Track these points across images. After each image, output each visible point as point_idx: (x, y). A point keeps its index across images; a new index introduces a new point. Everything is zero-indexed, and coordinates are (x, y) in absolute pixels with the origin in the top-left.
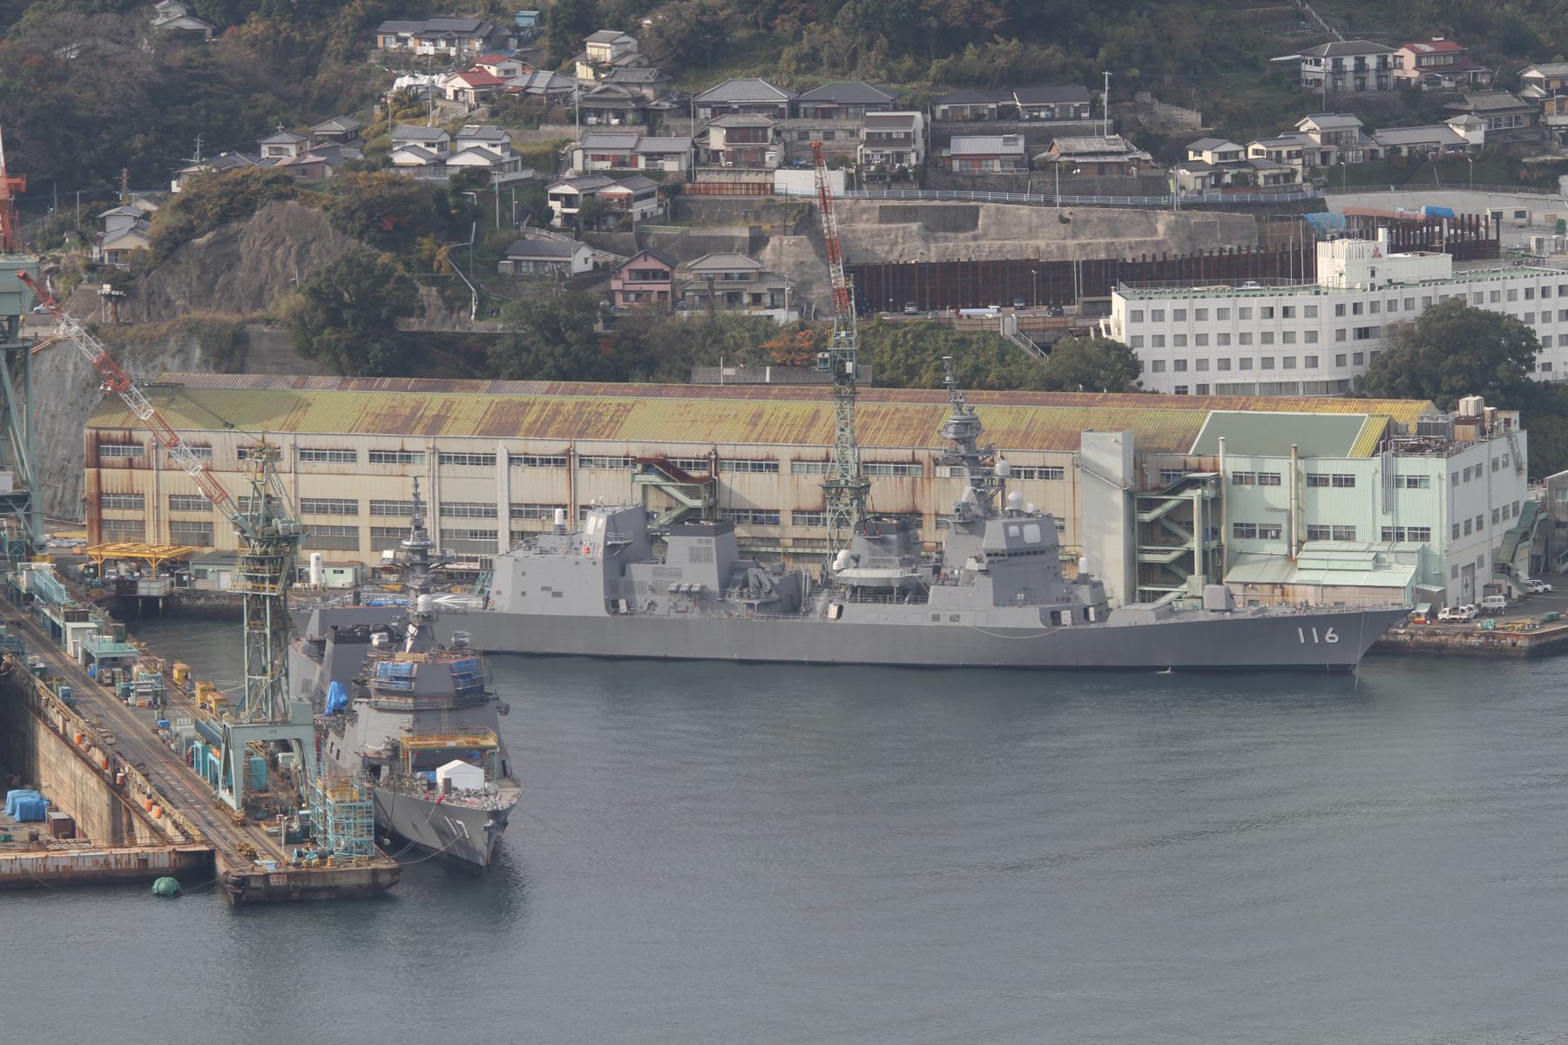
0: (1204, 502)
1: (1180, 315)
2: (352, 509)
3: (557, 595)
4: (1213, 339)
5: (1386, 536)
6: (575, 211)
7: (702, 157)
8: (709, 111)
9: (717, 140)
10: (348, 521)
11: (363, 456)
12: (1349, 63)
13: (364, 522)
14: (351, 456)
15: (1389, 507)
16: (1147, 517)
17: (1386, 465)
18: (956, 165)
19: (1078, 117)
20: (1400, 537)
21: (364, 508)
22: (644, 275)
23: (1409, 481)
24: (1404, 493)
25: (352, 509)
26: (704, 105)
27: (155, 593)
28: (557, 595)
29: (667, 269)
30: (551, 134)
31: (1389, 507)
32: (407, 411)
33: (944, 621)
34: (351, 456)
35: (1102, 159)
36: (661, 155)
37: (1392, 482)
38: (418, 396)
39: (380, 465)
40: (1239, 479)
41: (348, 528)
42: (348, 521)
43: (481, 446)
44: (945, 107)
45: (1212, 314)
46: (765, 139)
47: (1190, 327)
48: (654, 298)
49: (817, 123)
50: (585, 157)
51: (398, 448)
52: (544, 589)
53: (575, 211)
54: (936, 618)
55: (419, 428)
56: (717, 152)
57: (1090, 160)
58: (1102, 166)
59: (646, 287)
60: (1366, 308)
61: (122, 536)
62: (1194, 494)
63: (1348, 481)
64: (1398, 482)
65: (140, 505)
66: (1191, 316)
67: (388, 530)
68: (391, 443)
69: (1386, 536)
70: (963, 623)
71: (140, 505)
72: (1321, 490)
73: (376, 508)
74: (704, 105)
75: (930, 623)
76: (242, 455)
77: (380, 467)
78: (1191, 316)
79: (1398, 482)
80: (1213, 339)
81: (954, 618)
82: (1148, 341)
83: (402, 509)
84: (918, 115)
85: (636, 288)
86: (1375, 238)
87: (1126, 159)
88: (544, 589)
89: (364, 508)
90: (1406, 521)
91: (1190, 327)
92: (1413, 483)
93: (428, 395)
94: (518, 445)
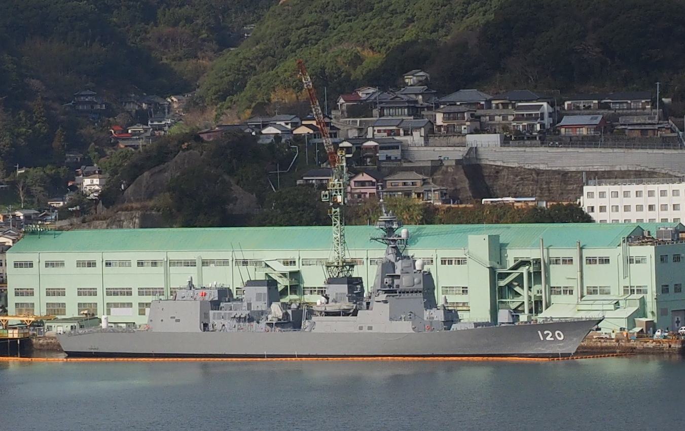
0: (529, 274)
1: (616, 195)
3: (178, 321)
4: (633, 208)
5: (626, 291)
6: (350, 156)
13: (135, 299)
16: (502, 283)
17: (625, 251)
18: (563, 130)
20: (632, 291)
21: (135, 292)
22: (363, 184)
27: (16, 336)
28: (178, 321)
29: (374, 180)
33: (365, 330)
35: (643, 127)
44: (569, 102)
45: (633, 194)
46: (464, 118)
47: (621, 201)
48: (367, 196)
50: (374, 131)
52: (171, 318)
54: (361, 328)
57: (637, 127)
59: (363, 191)
61: (24, 312)
63: (607, 261)
64: (631, 261)
65: (32, 294)
66: (621, 195)
69: (62, 264)
70: (374, 330)
71: (32, 294)
75: (357, 331)
79: (631, 261)
80: (633, 208)
81: (370, 328)
82: (597, 209)
83: (153, 292)
85: (358, 191)
87: (656, 127)
88: (171, 318)
89: (135, 292)
90: (635, 283)
91: (621, 201)
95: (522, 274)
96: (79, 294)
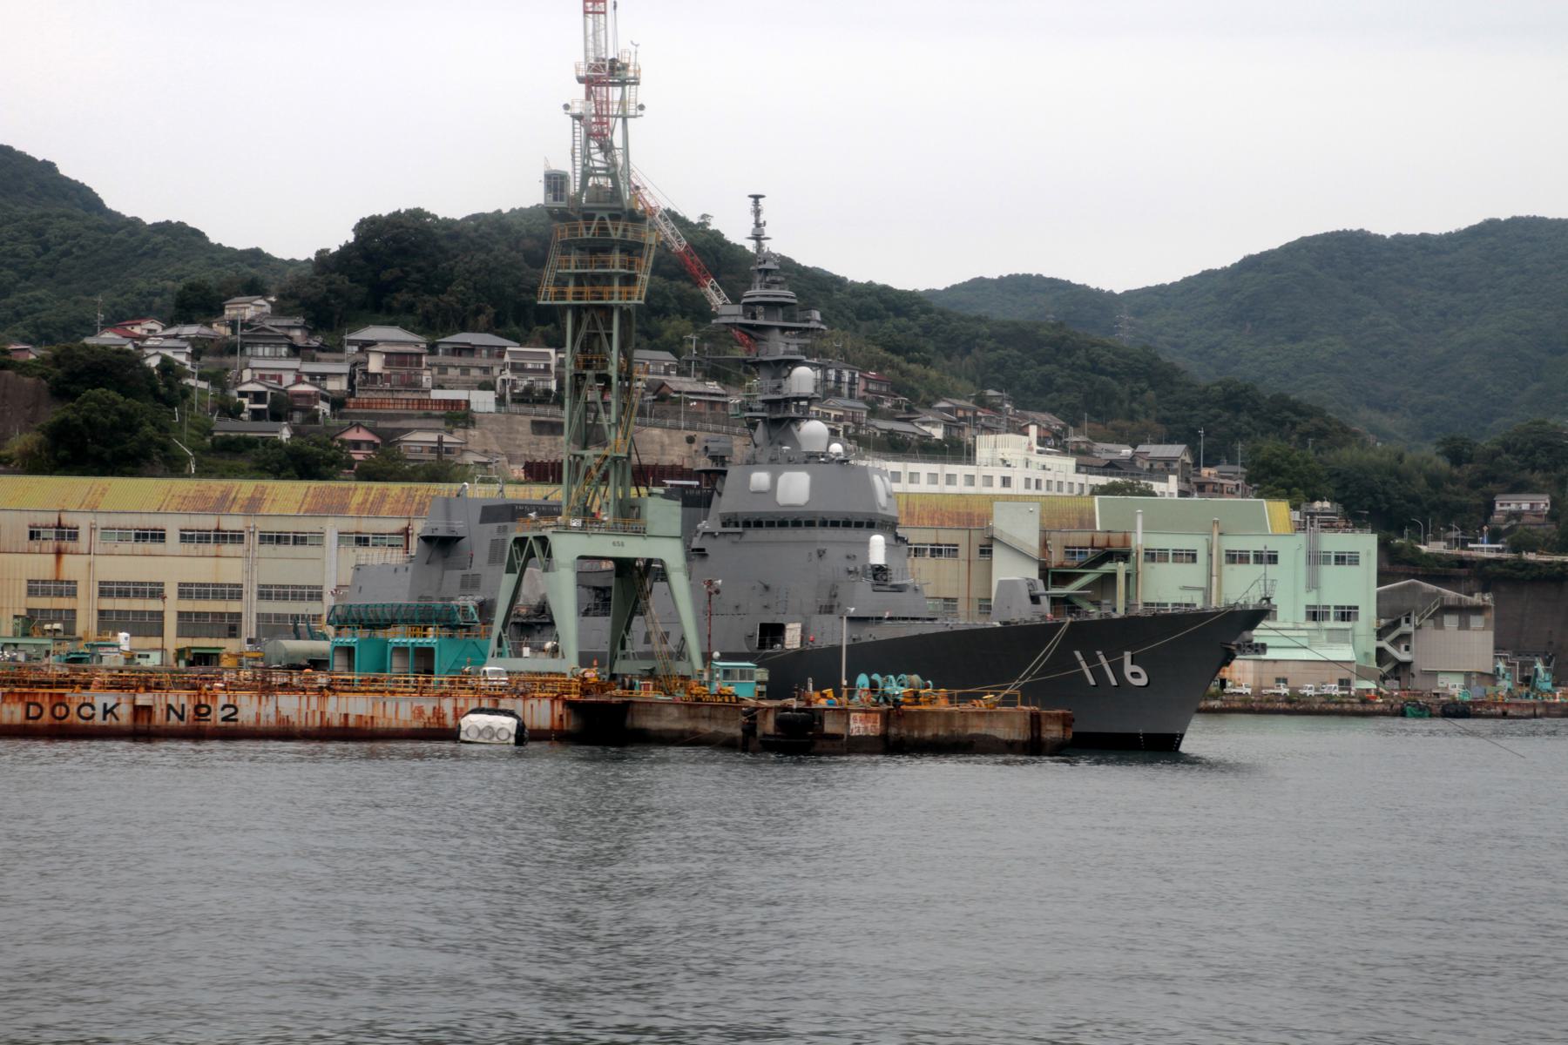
2: (157, 592)
7: (359, 378)
8: (356, 348)
9: (375, 364)
10: (153, 605)
11: (173, 536)
12: (832, 374)
13: (172, 607)
14: (159, 536)
15: (1313, 584)
19: (667, 373)
21: (171, 591)
23: (1337, 558)
24: (1330, 572)
25: (316, 595)
26: (351, 343)
30: (210, 364)
31: (1313, 584)
32: (218, 494)
34: (159, 536)
36: (324, 376)
37: (1316, 559)
38: (226, 482)
39: (192, 546)
40: (1151, 556)
41: (152, 613)
42: (153, 605)
43: (306, 525)
49: (456, 360)
51: (214, 526)
53: (264, 406)
55: (235, 509)
56: (375, 375)
58: (712, 403)
60: (1044, 485)
62: (1121, 568)
67: (198, 614)
68: (208, 522)
72: (1239, 568)
73: (185, 591)
74: (351, 343)
76: (33, 535)
77: (190, 548)
78: (905, 478)
84: (552, 351)
86: (1027, 434)
89: (171, 591)
92: (1340, 559)
93: (237, 483)
94: (350, 525)
95: (1112, 577)
96: (32, 592)
